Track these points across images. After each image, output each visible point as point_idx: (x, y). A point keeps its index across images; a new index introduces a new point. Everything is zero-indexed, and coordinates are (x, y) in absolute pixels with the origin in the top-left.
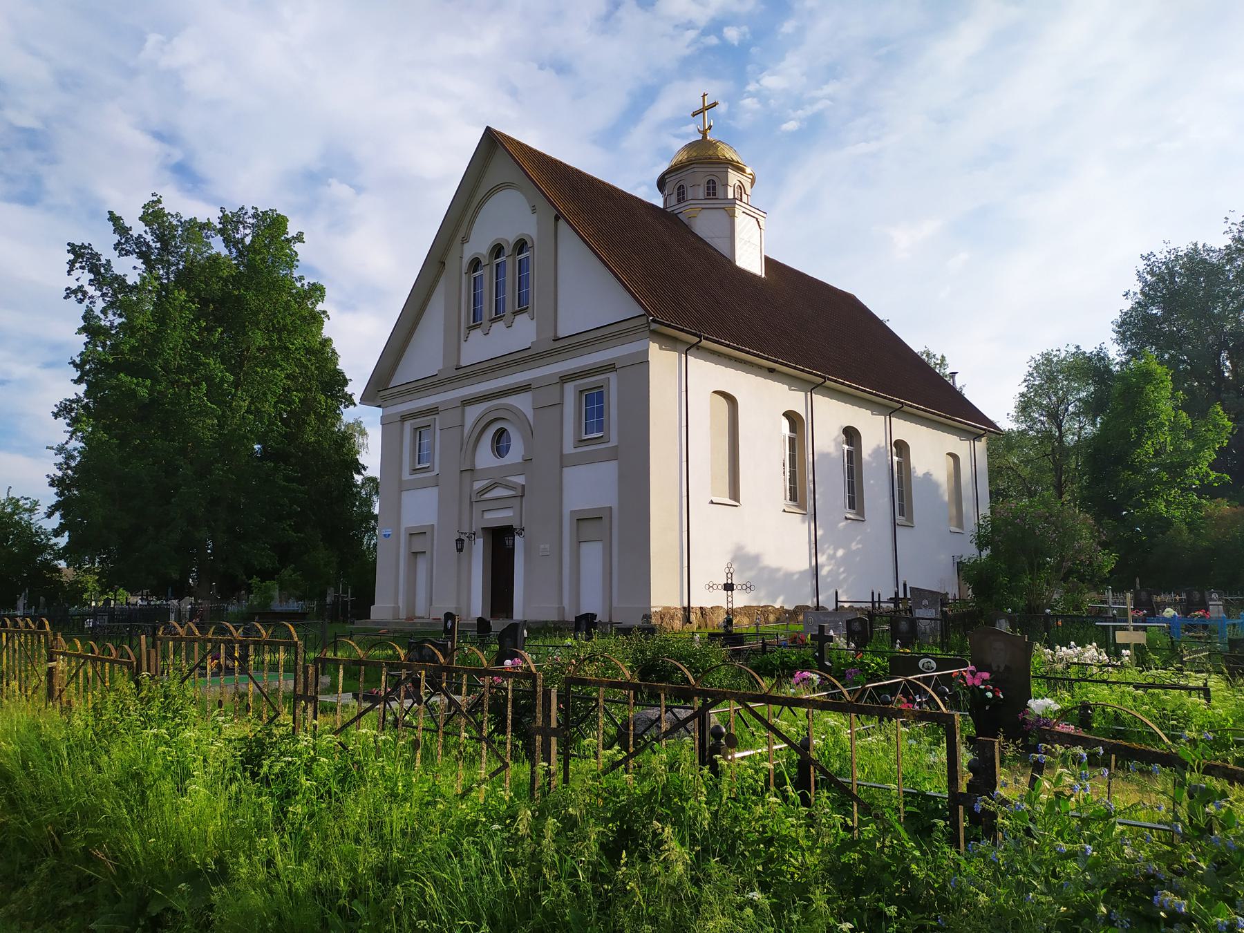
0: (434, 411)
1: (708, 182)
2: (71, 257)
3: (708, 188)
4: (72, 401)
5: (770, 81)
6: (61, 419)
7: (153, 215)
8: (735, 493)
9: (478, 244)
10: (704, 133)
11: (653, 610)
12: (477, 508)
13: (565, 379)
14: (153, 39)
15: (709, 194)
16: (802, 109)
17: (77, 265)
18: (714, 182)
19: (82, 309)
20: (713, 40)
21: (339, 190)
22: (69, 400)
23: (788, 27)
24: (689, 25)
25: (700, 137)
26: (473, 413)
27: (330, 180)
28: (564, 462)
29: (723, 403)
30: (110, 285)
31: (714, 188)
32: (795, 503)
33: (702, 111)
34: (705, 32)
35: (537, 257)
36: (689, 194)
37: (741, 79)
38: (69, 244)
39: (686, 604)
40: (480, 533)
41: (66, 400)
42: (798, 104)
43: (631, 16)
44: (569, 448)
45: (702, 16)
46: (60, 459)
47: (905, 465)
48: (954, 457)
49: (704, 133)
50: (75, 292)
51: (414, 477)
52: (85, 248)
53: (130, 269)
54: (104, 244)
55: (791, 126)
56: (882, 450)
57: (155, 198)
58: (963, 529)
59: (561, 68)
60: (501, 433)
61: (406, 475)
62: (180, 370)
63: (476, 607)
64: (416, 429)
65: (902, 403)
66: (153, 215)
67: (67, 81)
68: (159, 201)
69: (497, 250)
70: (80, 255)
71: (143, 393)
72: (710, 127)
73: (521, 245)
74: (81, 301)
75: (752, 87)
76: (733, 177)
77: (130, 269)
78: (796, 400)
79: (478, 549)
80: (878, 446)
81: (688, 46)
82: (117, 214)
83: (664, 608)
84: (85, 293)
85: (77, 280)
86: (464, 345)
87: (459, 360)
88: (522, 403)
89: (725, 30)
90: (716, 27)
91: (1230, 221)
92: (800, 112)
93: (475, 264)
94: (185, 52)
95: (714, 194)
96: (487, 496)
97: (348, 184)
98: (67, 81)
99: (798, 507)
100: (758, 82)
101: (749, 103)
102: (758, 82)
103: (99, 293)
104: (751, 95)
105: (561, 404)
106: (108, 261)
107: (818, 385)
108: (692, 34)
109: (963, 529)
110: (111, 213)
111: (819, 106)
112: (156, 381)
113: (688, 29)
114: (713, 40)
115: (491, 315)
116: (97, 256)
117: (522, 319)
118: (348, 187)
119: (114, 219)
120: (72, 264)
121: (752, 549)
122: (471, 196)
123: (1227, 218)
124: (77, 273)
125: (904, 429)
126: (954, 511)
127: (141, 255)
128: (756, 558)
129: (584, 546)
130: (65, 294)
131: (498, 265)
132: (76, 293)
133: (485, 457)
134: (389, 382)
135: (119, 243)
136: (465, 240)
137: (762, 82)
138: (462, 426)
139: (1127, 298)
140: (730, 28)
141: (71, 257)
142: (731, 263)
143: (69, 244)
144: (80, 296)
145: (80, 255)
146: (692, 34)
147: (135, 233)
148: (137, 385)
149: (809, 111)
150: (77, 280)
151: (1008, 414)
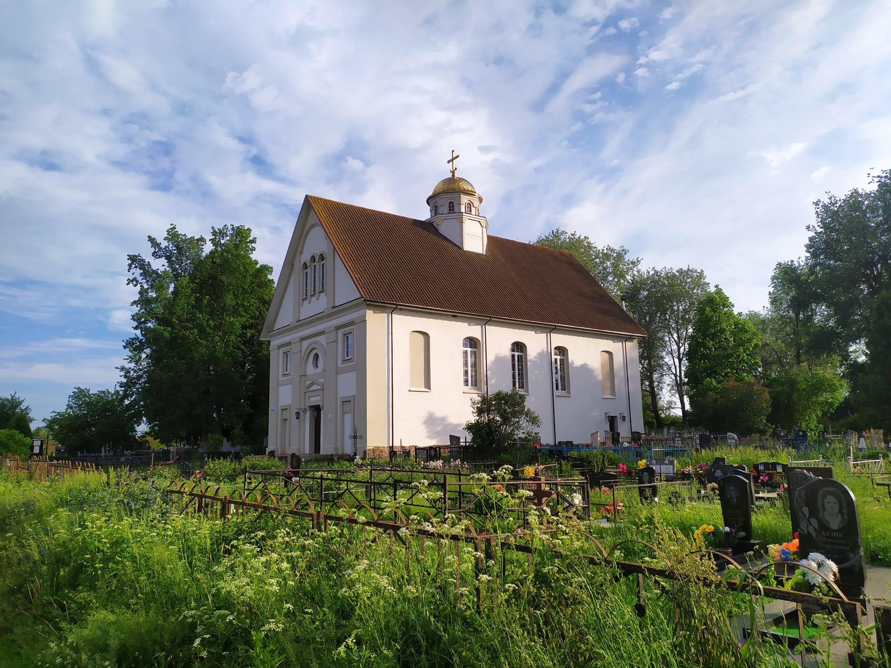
0: (289, 344)
1: (450, 203)
2: (130, 262)
3: (450, 207)
4: (133, 339)
5: (656, 55)
6: (127, 349)
7: (173, 235)
8: (428, 385)
9: (306, 257)
10: (453, 172)
11: (368, 448)
12: (308, 395)
13: (338, 328)
14: (231, 75)
15: (450, 210)
16: (682, 73)
17: (133, 266)
18: (453, 203)
19: (138, 288)
20: (611, 31)
21: (354, 164)
22: (132, 339)
23: (667, 14)
24: (594, 23)
25: (450, 175)
26: (306, 344)
27: (347, 158)
28: (338, 371)
29: (421, 337)
30: (150, 276)
31: (453, 206)
32: (475, 388)
33: (452, 160)
34: (605, 26)
35: (328, 262)
36: (440, 210)
37: (633, 53)
38: (128, 255)
39: (391, 445)
40: (308, 408)
41: (130, 339)
42: (679, 69)
43: (549, 20)
44: (340, 365)
45: (599, 14)
46: (123, 373)
47: (564, 362)
48: (610, 354)
49: (453, 172)
50: (132, 281)
51: (284, 378)
52: (137, 256)
53: (159, 265)
54: (146, 254)
55: (673, 86)
56: (545, 353)
57: (172, 226)
58: (615, 396)
59: (499, 61)
60: (316, 356)
61: (281, 378)
62: (187, 321)
63: (307, 449)
64: (284, 353)
65: (555, 326)
66: (173, 235)
67: (183, 109)
68: (174, 228)
69: (313, 259)
70: (135, 260)
71: (167, 335)
72: (456, 169)
73: (322, 257)
74: (136, 285)
75: (643, 60)
76: (465, 199)
77: (159, 265)
78: (475, 331)
79: (308, 417)
80: (543, 350)
81: (592, 39)
82: (153, 237)
83: (375, 447)
84: (137, 282)
85: (133, 274)
86: (301, 308)
87: (299, 318)
88: (322, 339)
89: (620, 23)
90: (613, 20)
91: (871, 176)
92: (680, 76)
93: (305, 266)
94: (252, 80)
95: (453, 210)
96: (310, 389)
97: (358, 159)
98: (183, 109)
99: (478, 390)
100: (646, 56)
101: (641, 72)
102: (646, 56)
103: (145, 281)
104: (641, 66)
105: (336, 341)
106: (149, 262)
107: (489, 321)
108: (594, 29)
109: (615, 396)
110: (149, 237)
111: (695, 69)
112: (173, 327)
113: (592, 26)
114: (611, 31)
115: (303, 296)
116: (143, 260)
117: (322, 295)
118: (358, 161)
119: (152, 240)
120: (130, 266)
121: (439, 414)
122: (303, 230)
123: (869, 174)
124: (132, 271)
125: (559, 340)
126: (608, 385)
127: (167, 258)
128: (443, 419)
129: (346, 415)
130: (127, 282)
131: (323, 264)
132: (133, 281)
133: (310, 369)
134: (273, 327)
135: (155, 252)
136: (301, 253)
137: (649, 57)
138: (301, 352)
139: (809, 230)
140: (623, 21)
141: (130, 262)
142: (460, 248)
143: (128, 255)
144: (135, 283)
145: (135, 260)
146: (594, 29)
147: (163, 246)
148: (164, 330)
149: (687, 73)
150: (133, 274)
151: (764, 307)
